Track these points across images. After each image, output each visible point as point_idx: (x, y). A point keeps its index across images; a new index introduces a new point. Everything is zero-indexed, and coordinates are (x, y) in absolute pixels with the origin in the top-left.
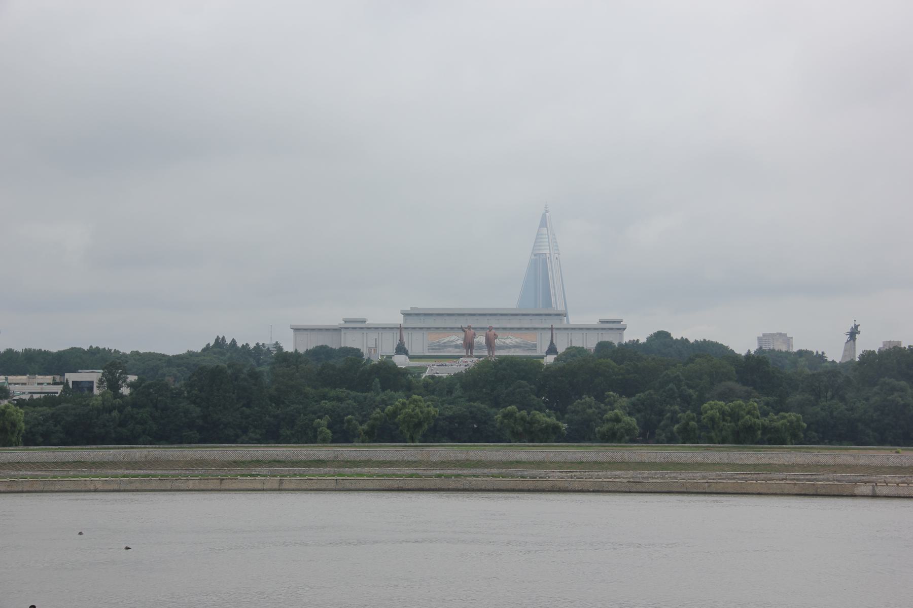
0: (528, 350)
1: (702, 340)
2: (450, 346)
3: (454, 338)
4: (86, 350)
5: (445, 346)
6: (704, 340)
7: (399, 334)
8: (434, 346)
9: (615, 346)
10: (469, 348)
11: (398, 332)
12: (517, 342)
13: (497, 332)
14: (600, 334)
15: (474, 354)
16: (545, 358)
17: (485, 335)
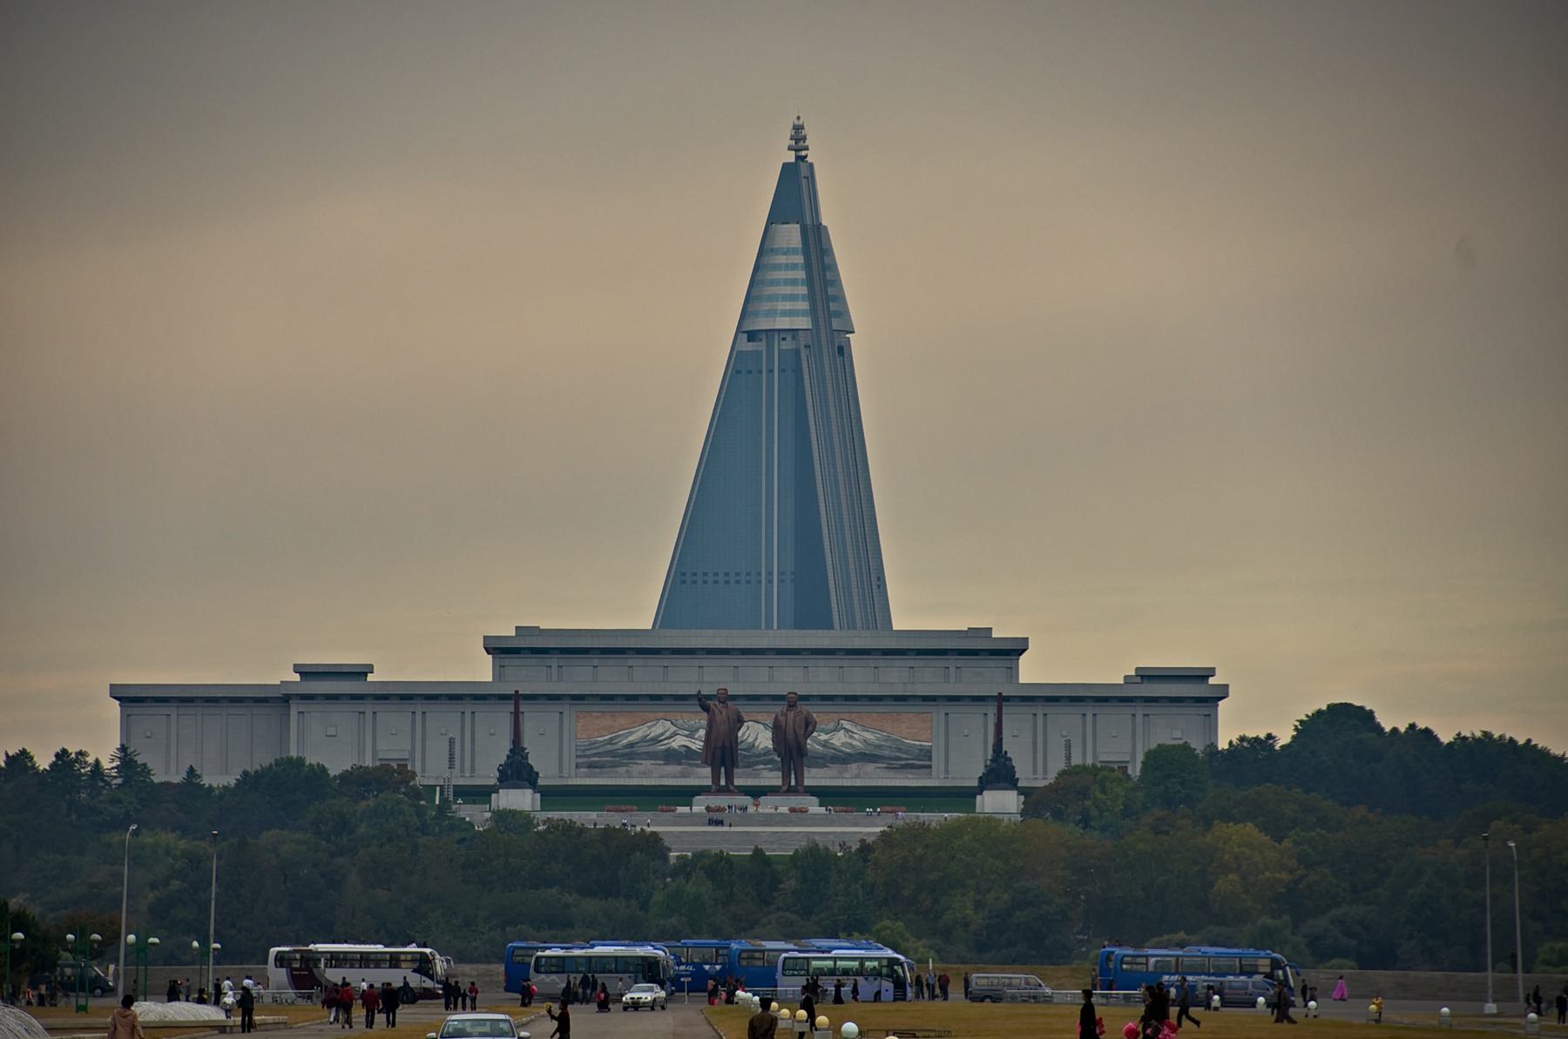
0: (903, 767)
1: (1478, 734)
3: (660, 730)
4: (48, 768)
5: (631, 754)
6: (1485, 733)
7: (992, 720)
8: (595, 755)
9: (1196, 756)
10: (723, 764)
11: (992, 711)
13: (817, 713)
14: (1139, 718)
15: (738, 782)
16: (494, 796)
17: (770, 722)
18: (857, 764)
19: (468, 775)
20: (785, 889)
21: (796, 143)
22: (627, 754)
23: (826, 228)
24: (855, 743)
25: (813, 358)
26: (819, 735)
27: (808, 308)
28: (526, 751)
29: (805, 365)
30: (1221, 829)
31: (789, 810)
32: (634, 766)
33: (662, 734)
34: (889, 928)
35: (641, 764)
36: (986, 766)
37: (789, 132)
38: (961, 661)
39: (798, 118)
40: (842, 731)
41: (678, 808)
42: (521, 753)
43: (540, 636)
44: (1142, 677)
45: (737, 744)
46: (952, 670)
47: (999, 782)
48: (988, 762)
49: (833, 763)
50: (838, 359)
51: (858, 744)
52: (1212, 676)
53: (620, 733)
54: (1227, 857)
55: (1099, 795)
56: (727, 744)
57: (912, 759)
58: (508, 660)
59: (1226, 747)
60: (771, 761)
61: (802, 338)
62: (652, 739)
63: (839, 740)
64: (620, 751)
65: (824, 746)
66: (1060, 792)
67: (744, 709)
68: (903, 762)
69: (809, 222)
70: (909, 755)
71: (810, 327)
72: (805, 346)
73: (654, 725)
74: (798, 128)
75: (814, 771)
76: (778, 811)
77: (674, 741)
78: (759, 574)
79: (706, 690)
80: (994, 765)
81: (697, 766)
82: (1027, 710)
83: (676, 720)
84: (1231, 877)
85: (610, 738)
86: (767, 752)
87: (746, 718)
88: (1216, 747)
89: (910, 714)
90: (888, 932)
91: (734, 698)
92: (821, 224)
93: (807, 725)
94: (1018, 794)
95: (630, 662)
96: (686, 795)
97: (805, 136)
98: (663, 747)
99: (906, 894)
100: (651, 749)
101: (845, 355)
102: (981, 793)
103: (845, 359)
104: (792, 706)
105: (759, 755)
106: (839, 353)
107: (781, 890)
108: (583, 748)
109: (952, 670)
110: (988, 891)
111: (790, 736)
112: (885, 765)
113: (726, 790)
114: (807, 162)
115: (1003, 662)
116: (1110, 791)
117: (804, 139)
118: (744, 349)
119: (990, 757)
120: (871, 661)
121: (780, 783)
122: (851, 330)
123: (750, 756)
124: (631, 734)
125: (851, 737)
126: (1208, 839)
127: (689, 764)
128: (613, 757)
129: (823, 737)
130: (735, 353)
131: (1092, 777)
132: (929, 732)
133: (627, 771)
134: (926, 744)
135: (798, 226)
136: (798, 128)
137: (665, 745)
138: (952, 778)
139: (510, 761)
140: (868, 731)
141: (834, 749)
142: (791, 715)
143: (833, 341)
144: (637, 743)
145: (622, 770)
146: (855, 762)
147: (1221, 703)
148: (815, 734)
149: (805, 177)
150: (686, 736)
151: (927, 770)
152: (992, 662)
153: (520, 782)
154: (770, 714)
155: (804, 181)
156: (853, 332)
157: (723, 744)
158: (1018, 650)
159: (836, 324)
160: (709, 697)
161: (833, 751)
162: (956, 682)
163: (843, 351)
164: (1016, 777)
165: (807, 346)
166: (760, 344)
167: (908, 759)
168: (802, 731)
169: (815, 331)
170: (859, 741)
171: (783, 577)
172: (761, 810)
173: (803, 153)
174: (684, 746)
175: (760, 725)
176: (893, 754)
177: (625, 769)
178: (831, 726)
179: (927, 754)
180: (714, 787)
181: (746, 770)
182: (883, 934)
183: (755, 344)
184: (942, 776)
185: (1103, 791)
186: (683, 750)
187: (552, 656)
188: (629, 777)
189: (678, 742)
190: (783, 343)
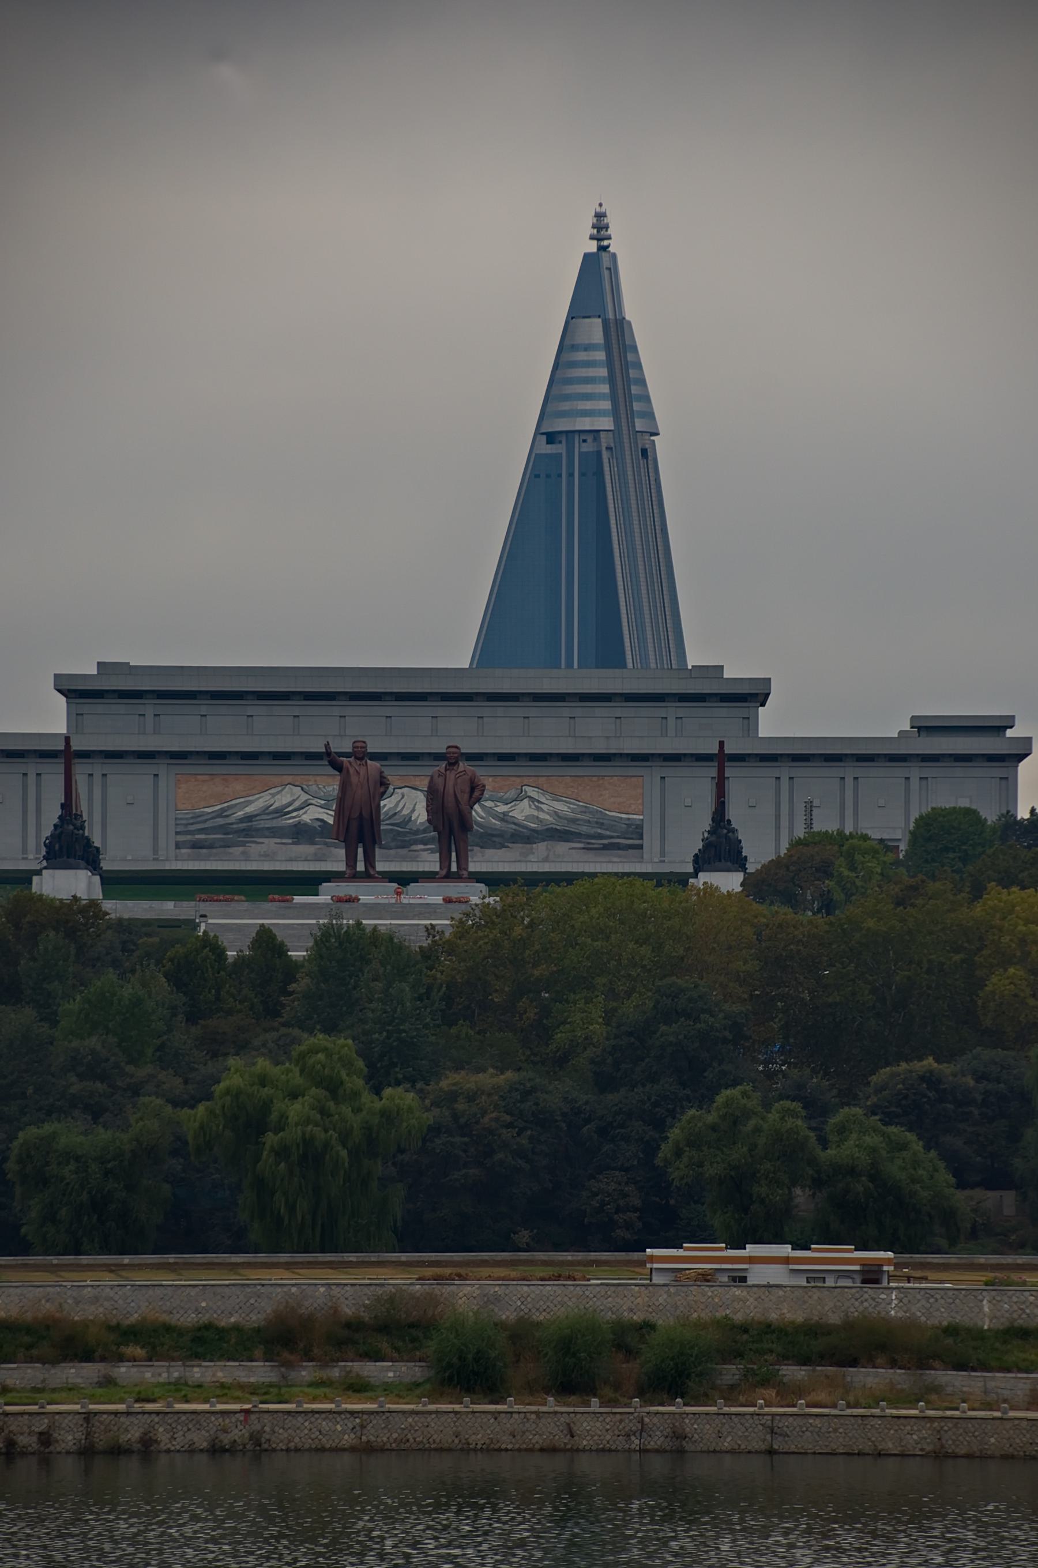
0: (605, 847)
2: (274, 832)
3: (285, 800)
10: (361, 839)
12: (556, 814)
13: (486, 776)
14: (915, 783)
15: (381, 866)
16: (35, 879)
17: (424, 783)
19: (31, 857)
21: (598, 232)
23: (629, 323)
24: (542, 816)
25: (615, 460)
27: (610, 407)
29: (606, 468)
30: (997, 896)
32: (253, 845)
33: (290, 804)
34: (325, 1049)
35: (263, 843)
37: (590, 220)
39: (601, 205)
40: (526, 801)
42: (75, 822)
43: (130, 674)
44: (920, 728)
46: (671, 722)
47: (720, 861)
50: (641, 462)
51: (548, 817)
52: (1011, 727)
53: (233, 802)
54: (1006, 939)
55: (846, 873)
56: (365, 814)
57: (618, 837)
58: (88, 707)
59: (1027, 816)
62: (276, 811)
63: (522, 811)
64: (235, 826)
65: (502, 820)
66: (792, 868)
67: (393, 773)
68: (606, 842)
69: (611, 316)
70: (614, 832)
71: (612, 428)
72: (607, 448)
73: (278, 792)
74: (600, 216)
75: (490, 852)
77: (305, 813)
80: (713, 838)
83: (308, 786)
84: (1011, 970)
86: (425, 831)
88: (1016, 817)
90: (321, 1056)
92: (624, 318)
93: (473, 789)
95: (250, 711)
96: (311, 882)
97: (608, 224)
98: (291, 821)
100: (275, 823)
103: (649, 462)
106: (642, 455)
109: (671, 722)
110: (629, 995)
111: (450, 801)
112: (581, 845)
113: (368, 876)
114: (609, 251)
116: (860, 867)
117: (607, 228)
118: (543, 452)
120: (565, 710)
121: (437, 869)
123: (405, 834)
124: (249, 803)
125: (538, 809)
126: (978, 910)
127: (326, 844)
128: (225, 834)
129: (502, 808)
130: (533, 455)
131: (836, 848)
132: (640, 801)
133: (243, 853)
134: (635, 817)
135: (600, 320)
136: (600, 216)
138: (669, 862)
139: (58, 832)
141: (515, 824)
142: (451, 776)
144: (257, 815)
146: (544, 840)
147: (1023, 766)
149: (607, 268)
152: (723, 711)
153: (72, 860)
154: (423, 775)
155: (606, 273)
156: (657, 434)
157: (361, 814)
160: (347, 755)
161: (514, 827)
163: (646, 454)
164: (744, 854)
166: (560, 445)
167: (612, 837)
168: (466, 796)
169: (616, 432)
170: (548, 813)
173: (605, 243)
174: (318, 819)
175: (419, 792)
176: (592, 831)
177: (241, 849)
178: (512, 794)
179: (637, 830)
182: (311, 1061)
185: (852, 868)
186: (317, 824)
187: (146, 701)
188: (246, 860)
189: (308, 816)
190: (584, 444)
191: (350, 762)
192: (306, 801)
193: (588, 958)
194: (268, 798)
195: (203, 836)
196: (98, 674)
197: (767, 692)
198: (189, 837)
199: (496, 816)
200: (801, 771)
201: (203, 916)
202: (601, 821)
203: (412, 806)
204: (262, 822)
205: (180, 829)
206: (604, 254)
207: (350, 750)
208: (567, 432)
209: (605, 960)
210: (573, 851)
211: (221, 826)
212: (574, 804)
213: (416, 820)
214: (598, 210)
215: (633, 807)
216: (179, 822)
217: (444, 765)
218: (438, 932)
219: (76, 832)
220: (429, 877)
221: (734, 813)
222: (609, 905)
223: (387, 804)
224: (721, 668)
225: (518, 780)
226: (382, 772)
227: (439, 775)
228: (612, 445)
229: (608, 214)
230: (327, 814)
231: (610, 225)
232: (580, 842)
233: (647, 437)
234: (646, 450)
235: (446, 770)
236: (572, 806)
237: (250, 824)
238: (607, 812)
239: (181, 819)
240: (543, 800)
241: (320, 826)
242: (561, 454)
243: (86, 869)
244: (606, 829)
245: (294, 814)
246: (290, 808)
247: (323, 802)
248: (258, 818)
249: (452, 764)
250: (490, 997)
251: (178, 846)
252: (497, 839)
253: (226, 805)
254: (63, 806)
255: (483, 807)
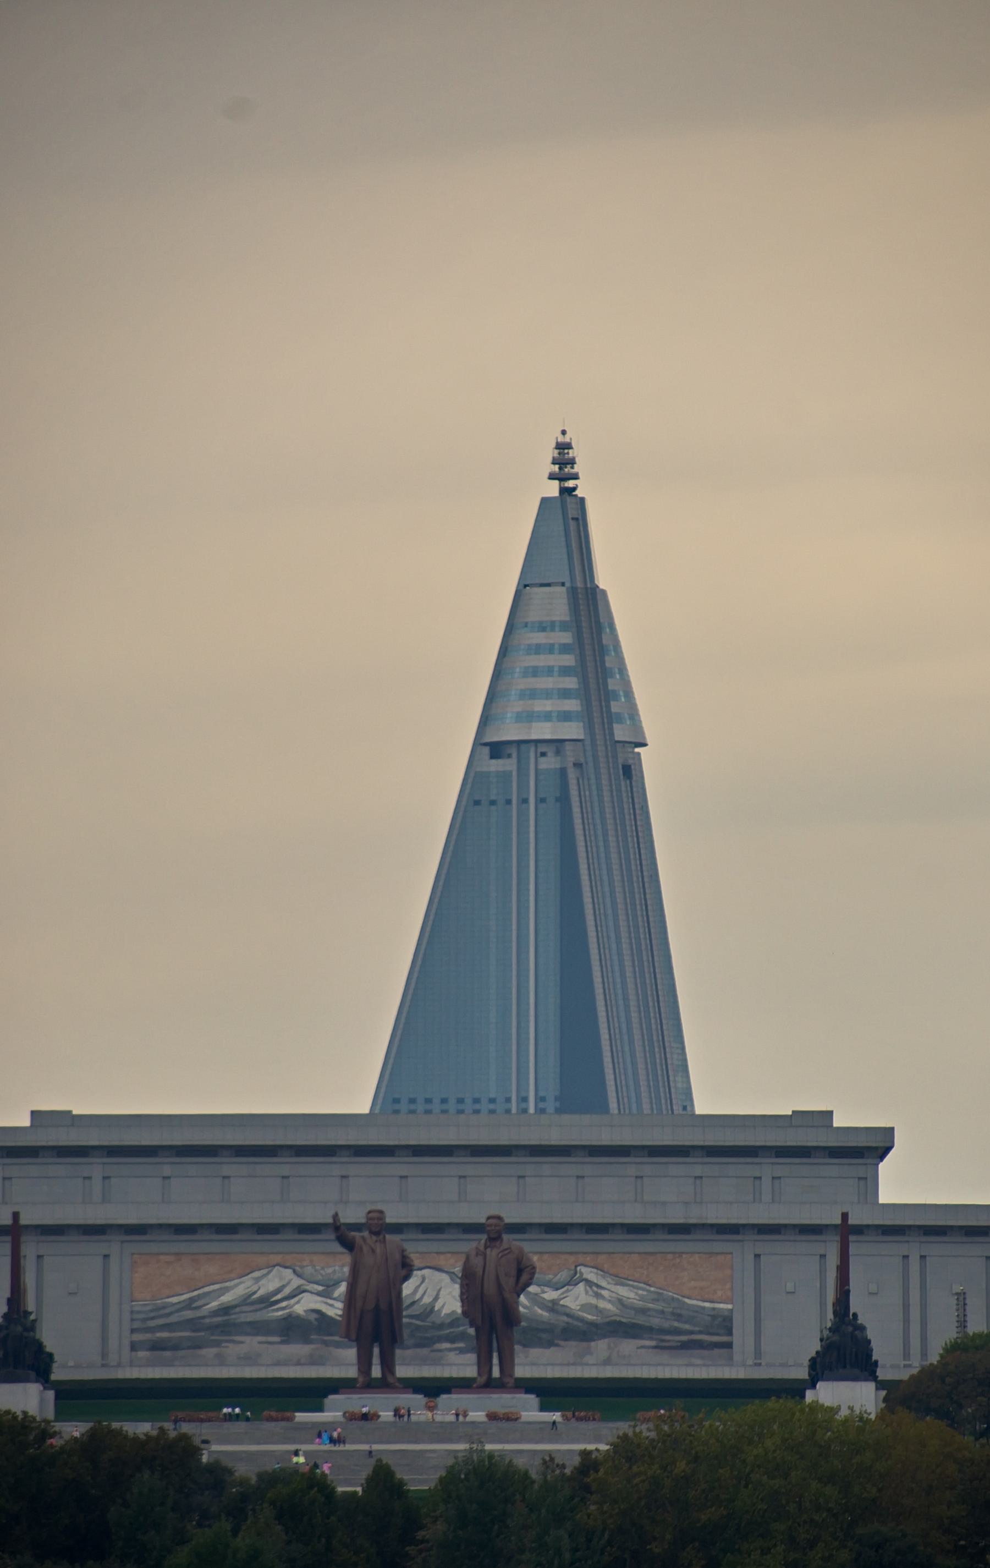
0: (685, 1346)
2: (258, 1328)
7: (833, 1261)
12: (620, 1302)
15: (402, 1371)
17: (458, 1270)
18: (606, 1340)
20: (427, 1541)
21: (560, 469)
22: (217, 1326)
23: (604, 592)
24: (602, 1304)
25: (586, 781)
26: (544, 1292)
28: (32, 1317)
31: (487, 1416)
32: (231, 1345)
33: (278, 1291)
35: (242, 1342)
36: (821, 1340)
37: (550, 452)
38: (783, 1167)
39: (564, 432)
40: (581, 1285)
41: (297, 1414)
45: (400, 1310)
46: (766, 1183)
47: (845, 1367)
48: (826, 1333)
49: (566, 1340)
50: (623, 784)
51: (609, 1306)
53: (207, 1289)
57: (700, 1332)
60: (463, 1336)
61: (571, 755)
63: (577, 1298)
64: (207, 1321)
66: (948, 1380)
67: (415, 1249)
68: (684, 1338)
71: (581, 737)
72: (575, 764)
74: (563, 447)
75: (535, 1352)
76: (468, 1419)
77: (298, 1302)
78: (508, 1100)
79: (352, 1215)
80: (836, 1338)
81: (337, 1345)
82: (893, 1249)
85: (190, 1299)
86: (454, 1323)
87: (417, 1262)
89: (697, 1256)
91: (398, 1228)
93: (520, 1272)
94: (877, 1389)
95: (226, 1170)
98: (280, 1313)
99: (657, 1550)
100: (259, 1316)
101: (634, 778)
102: (813, 1386)
104: (494, 1239)
105: (441, 1326)
106: (624, 774)
107: (422, 1542)
108: (142, 1316)
109: (766, 1183)
111: (490, 1288)
112: (653, 1343)
113: (386, 1384)
114: (576, 496)
115: (850, 1168)
117: (572, 462)
119: (829, 1325)
120: (630, 1167)
122: (642, 741)
124: (226, 1290)
125: (598, 1296)
128: (194, 1331)
129: (550, 1295)
130: (472, 775)
132: (728, 1286)
133: (218, 1356)
134: (722, 1306)
136: (563, 447)
137: (283, 1308)
140: (623, 1285)
142: (492, 1254)
143: (615, 757)
144: (235, 1306)
145: (210, 1352)
146: (604, 1336)
148: (532, 1289)
149: (573, 519)
150: (319, 1294)
151: (724, 1351)
152: (834, 1168)
156: (645, 745)
158: (876, 1148)
159: (620, 733)
160: (357, 1227)
161: (565, 1318)
162: (773, 1201)
164: (874, 1358)
165: (577, 765)
167: (692, 1333)
168: (512, 1281)
170: (610, 1301)
171: (541, 1105)
172: (438, 1418)
173: (571, 484)
176: (666, 1325)
177: (214, 1351)
178: (563, 1276)
179: (725, 1324)
180: (361, 1379)
181: (419, 1350)
183: (500, 761)
184: (750, 1362)
186: (313, 1317)
189: (304, 1305)
190: (542, 760)
191: (364, 1239)
192: (299, 1287)
193: (762, 1500)
194: (249, 1283)
195: (165, 1335)
196: (32, 1125)
197: (888, 1145)
198: (148, 1336)
199: (543, 1305)
200: (936, 1249)
201: (206, 1442)
202: (679, 1311)
203: (435, 1293)
204: (243, 1315)
205: (136, 1325)
206: (569, 499)
207: (363, 1221)
208: (519, 743)
209: (784, 1502)
210: (643, 1350)
211: (190, 1321)
212: (643, 1289)
213: (440, 1310)
214: (561, 439)
215: (719, 1293)
216: (135, 1316)
217: (483, 1242)
218: (558, 1465)
219: (26, 1334)
220: (463, 1385)
221: (856, 1304)
222: (786, 1436)
223: (407, 1288)
224: (829, 1114)
225: (572, 1259)
226: (403, 1251)
227: (477, 1255)
228: (582, 760)
229: (573, 445)
230: (326, 1303)
231: (577, 460)
232: (651, 1339)
233: (630, 750)
234: (630, 766)
235: (486, 1247)
236: (640, 1292)
237: (226, 1318)
238: (687, 1300)
239: (138, 1312)
240: (604, 1284)
241: (316, 1319)
242: (511, 772)
243: (37, 1381)
244: (685, 1322)
245: (284, 1304)
246: (279, 1297)
247: (320, 1288)
248: (237, 1310)
249: (494, 1239)
250: (648, 1547)
251: (134, 1347)
252: (544, 1336)
253: (196, 1293)
254: (9, 1301)
255: (529, 1296)
